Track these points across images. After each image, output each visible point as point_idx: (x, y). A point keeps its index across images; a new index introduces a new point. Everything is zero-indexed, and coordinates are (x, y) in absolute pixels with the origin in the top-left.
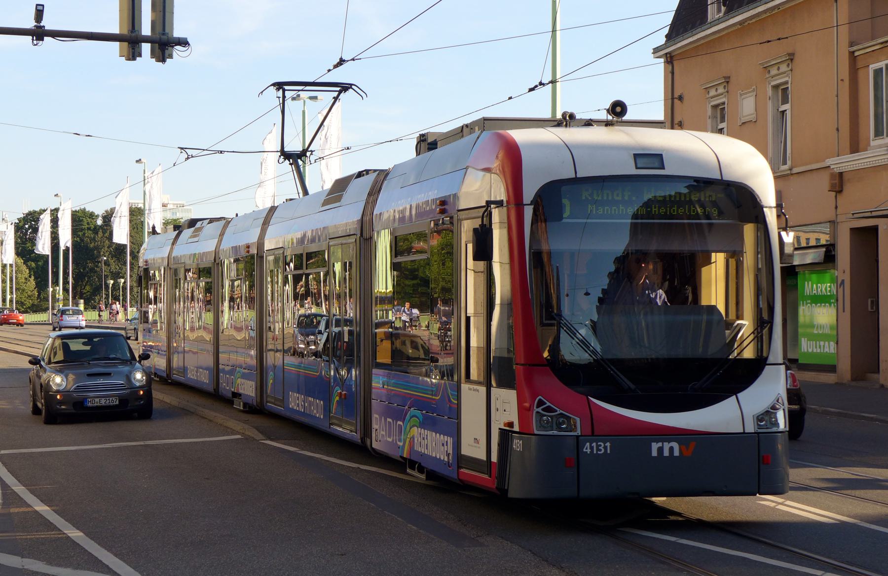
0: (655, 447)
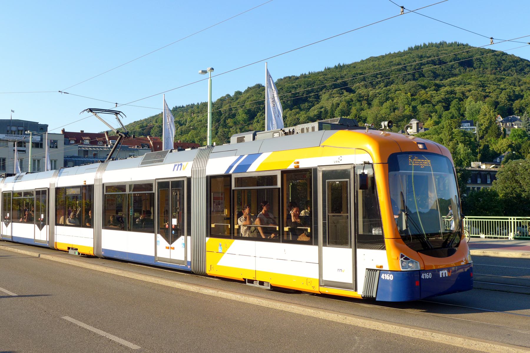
0: (441, 273)
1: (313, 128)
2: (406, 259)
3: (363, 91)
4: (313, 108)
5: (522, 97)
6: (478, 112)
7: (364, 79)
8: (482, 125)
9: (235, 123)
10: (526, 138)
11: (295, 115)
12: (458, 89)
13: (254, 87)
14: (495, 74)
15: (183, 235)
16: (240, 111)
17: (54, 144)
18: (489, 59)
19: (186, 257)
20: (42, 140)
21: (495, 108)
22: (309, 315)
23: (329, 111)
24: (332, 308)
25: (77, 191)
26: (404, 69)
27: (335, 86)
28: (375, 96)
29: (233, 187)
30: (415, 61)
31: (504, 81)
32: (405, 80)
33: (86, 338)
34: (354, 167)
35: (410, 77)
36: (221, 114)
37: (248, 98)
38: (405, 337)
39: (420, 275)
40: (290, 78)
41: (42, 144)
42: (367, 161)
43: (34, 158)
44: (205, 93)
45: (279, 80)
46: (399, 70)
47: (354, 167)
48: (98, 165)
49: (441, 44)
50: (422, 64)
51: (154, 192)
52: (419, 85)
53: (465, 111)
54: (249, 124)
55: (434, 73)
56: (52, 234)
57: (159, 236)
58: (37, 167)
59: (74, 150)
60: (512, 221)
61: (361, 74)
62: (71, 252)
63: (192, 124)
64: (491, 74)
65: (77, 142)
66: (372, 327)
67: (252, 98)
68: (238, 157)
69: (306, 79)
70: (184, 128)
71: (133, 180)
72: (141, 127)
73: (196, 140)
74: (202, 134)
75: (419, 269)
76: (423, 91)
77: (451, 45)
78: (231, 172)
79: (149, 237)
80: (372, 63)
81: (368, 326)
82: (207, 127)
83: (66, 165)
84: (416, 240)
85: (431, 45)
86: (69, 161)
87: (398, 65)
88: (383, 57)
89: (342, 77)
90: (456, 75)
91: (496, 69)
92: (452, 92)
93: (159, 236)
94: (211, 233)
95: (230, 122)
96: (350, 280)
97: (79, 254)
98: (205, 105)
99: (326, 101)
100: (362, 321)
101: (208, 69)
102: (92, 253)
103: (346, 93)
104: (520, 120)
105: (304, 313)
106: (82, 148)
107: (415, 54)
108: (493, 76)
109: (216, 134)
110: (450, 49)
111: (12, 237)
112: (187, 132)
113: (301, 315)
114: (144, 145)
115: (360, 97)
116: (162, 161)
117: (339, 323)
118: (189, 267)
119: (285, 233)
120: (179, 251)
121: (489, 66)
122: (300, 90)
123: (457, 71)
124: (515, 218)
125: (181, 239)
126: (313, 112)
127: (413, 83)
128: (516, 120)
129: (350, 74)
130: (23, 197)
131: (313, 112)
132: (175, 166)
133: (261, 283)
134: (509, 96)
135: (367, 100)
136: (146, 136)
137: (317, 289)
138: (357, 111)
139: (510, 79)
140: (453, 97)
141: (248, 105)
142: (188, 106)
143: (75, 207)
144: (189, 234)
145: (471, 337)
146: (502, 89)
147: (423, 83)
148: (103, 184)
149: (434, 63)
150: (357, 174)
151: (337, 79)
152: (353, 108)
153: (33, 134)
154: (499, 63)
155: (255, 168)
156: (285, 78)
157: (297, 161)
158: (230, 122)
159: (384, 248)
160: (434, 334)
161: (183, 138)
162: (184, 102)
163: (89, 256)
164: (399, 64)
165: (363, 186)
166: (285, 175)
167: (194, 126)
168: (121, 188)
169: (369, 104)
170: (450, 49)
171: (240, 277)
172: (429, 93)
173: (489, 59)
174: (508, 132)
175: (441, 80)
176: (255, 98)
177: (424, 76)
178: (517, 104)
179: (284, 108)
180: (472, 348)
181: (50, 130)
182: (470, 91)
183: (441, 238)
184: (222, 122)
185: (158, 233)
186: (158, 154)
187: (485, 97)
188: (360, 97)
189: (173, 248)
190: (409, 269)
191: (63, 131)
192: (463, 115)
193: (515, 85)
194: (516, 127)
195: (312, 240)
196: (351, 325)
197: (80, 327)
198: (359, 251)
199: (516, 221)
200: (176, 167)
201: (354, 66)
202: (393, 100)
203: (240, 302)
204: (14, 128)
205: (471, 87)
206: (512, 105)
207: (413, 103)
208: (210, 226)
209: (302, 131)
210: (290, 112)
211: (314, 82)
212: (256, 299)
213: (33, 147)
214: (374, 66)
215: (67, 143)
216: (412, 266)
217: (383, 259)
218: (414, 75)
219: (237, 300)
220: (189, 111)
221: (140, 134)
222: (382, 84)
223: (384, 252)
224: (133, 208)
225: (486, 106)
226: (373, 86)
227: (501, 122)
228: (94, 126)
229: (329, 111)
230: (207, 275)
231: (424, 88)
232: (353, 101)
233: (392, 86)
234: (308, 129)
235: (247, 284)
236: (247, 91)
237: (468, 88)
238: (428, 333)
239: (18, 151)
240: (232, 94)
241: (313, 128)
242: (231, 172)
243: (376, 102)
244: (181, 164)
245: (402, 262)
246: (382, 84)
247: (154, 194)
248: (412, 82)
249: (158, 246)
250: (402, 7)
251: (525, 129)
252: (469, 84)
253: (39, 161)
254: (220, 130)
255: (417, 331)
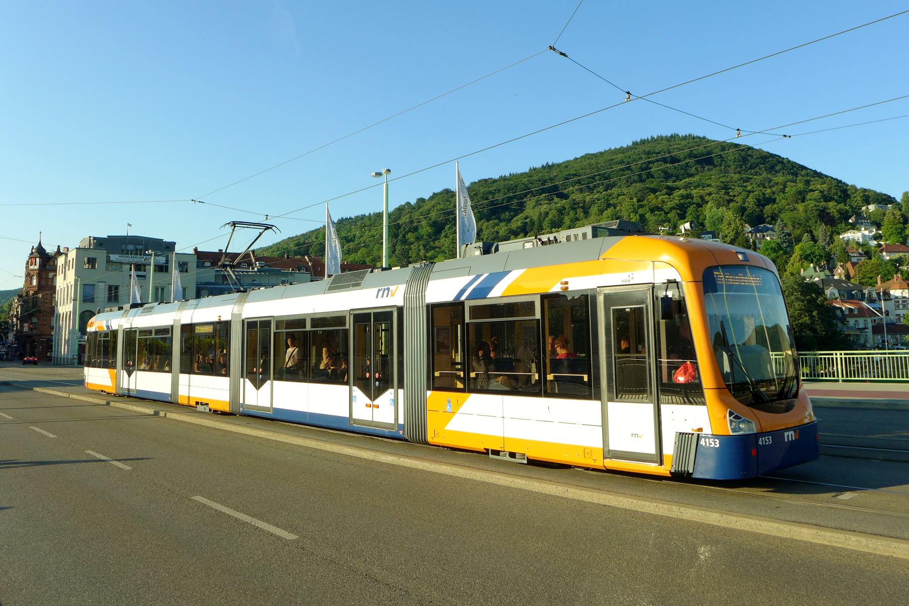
1: (584, 235)
2: (737, 417)
3: (577, 197)
4: (515, 218)
5: (774, 201)
6: (721, 220)
7: (579, 182)
8: (726, 236)
9: (418, 239)
10: (781, 252)
11: (494, 227)
12: (694, 192)
13: (441, 193)
14: (739, 173)
15: (392, 388)
16: (424, 223)
17: (183, 267)
18: (731, 154)
19: (397, 419)
20: (167, 261)
21: (742, 215)
22: (519, 487)
23: (536, 223)
24: (549, 478)
25: (209, 329)
26: (629, 168)
27: (543, 191)
28: (593, 202)
29: (467, 320)
30: (641, 158)
31: (752, 181)
32: (629, 183)
33: (224, 525)
34: (653, 288)
35: (636, 178)
36: (400, 228)
37: (434, 207)
38: (645, 513)
39: (757, 441)
40: (486, 180)
41: (167, 268)
42: (672, 278)
43: (157, 285)
44: (379, 201)
45: (472, 184)
46: (622, 170)
47: (653, 288)
48: (236, 295)
49: (672, 136)
50: (650, 162)
51: (347, 327)
52: (647, 188)
53: (705, 219)
54: (434, 240)
55: (665, 172)
56: (175, 384)
57: (355, 389)
58: (161, 297)
59: (209, 274)
60: (839, 356)
61: (575, 175)
62: (200, 408)
63: (362, 239)
64: (735, 173)
65: (214, 264)
66: (602, 502)
67: (439, 207)
68: (474, 276)
69: (507, 182)
70: (352, 245)
71: (316, 311)
72: (297, 245)
73: (368, 260)
74: (375, 253)
75: (755, 431)
76: (652, 196)
77: (685, 138)
78: (463, 298)
79: (341, 391)
80: (588, 161)
81: (596, 501)
82: (382, 244)
83: (198, 296)
84: (744, 391)
85: (661, 138)
86: (203, 289)
87: (620, 163)
88: (601, 153)
89: (551, 179)
90: (692, 175)
91: (741, 167)
92: (689, 196)
93: (357, 391)
94: (435, 384)
95: (411, 237)
96: (650, 448)
97: (210, 410)
98: (379, 216)
99: (532, 210)
100: (589, 493)
101: (383, 171)
102: (227, 409)
103: (556, 199)
104: (772, 230)
105: (512, 486)
106: (219, 273)
107: (640, 149)
108: (737, 176)
109: (394, 252)
110: (684, 143)
111: (128, 389)
112: (356, 250)
113: (509, 488)
114: (300, 266)
115: (575, 204)
116: (359, 285)
117: (559, 497)
118: (401, 432)
119: (548, 384)
120: (386, 410)
121: (731, 163)
122: (499, 197)
123: (693, 170)
124: (843, 352)
125: (389, 394)
126: (516, 223)
127: (639, 185)
128: (768, 229)
129: (560, 175)
130: (153, 336)
131: (516, 223)
132: (379, 291)
133: (513, 455)
134: (759, 200)
135: (583, 207)
136: (304, 256)
137: (599, 463)
138: (571, 221)
139: (758, 178)
140: (690, 203)
141: (433, 215)
142: (357, 217)
143: (203, 351)
144: (401, 385)
145: (730, 512)
146: (749, 192)
147: (652, 186)
148: (243, 321)
149: (665, 160)
150: (657, 298)
151: (545, 181)
152: (566, 218)
153: (156, 255)
154: (744, 160)
155: (498, 293)
156: (480, 181)
157: (564, 280)
158: (411, 237)
159: (704, 404)
160: (682, 509)
161: (351, 258)
162: (352, 212)
163: (224, 413)
164: (622, 162)
165: (666, 315)
166: (546, 301)
167: (364, 242)
168: (265, 324)
169: (586, 213)
170: (684, 143)
171: (481, 447)
172: (660, 198)
173: (731, 154)
174: (758, 246)
175: (674, 181)
176: (442, 206)
177: (652, 177)
178: (768, 209)
179: (478, 220)
180: (732, 526)
181: (178, 249)
182: (710, 194)
183: (773, 388)
184: (400, 237)
185: (354, 385)
186: (352, 275)
187: (729, 201)
188: (575, 204)
189: (378, 407)
190: (741, 433)
191: (196, 250)
192: (702, 225)
193: (764, 187)
194: (768, 238)
195: (588, 391)
196: (574, 500)
197: (216, 510)
198: (664, 408)
199: (843, 356)
200: (381, 292)
201: (566, 165)
202: (615, 208)
203: (429, 472)
204: (131, 247)
205: (711, 189)
206: (762, 211)
207: (641, 211)
208: (433, 374)
209: (568, 238)
210: (486, 223)
211: (516, 186)
212: (449, 468)
213: (155, 271)
214: (590, 165)
215: (200, 265)
216: (745, 429)
217: (700, 420)
218: (640, 176)
219: (425, 469)
220: (359, 223)
221: (296, 253)
222: (601, 188)
223: (703, 409)
224: (319, 350)
225: (730, 213)
226: (591, 190)
227: (750, 232)
228: (240, 243)
229: (536, 223)
230: (426, 443)
231: (654, 191)
232: (565, 209)
233: (614, 189)
234: (576, 236)
235: (491, 456)
236: (432, 198)
237: (707, 192)
238: (675, 508)
239: (138, 276)
240: (413, 202)
241: (584, 235)
242: (463, 298)
243: (594, 210)
244: (388, 289)
245: (731, 421)
246: (601, 188)
247: (346, 332)
248: (638, 184)
249: (354, 404)
250: (628, 93)
251: (779, 241)
252: (709, 186)
253: (163, 289)
254: (398, 247)
255: (661, 505)
